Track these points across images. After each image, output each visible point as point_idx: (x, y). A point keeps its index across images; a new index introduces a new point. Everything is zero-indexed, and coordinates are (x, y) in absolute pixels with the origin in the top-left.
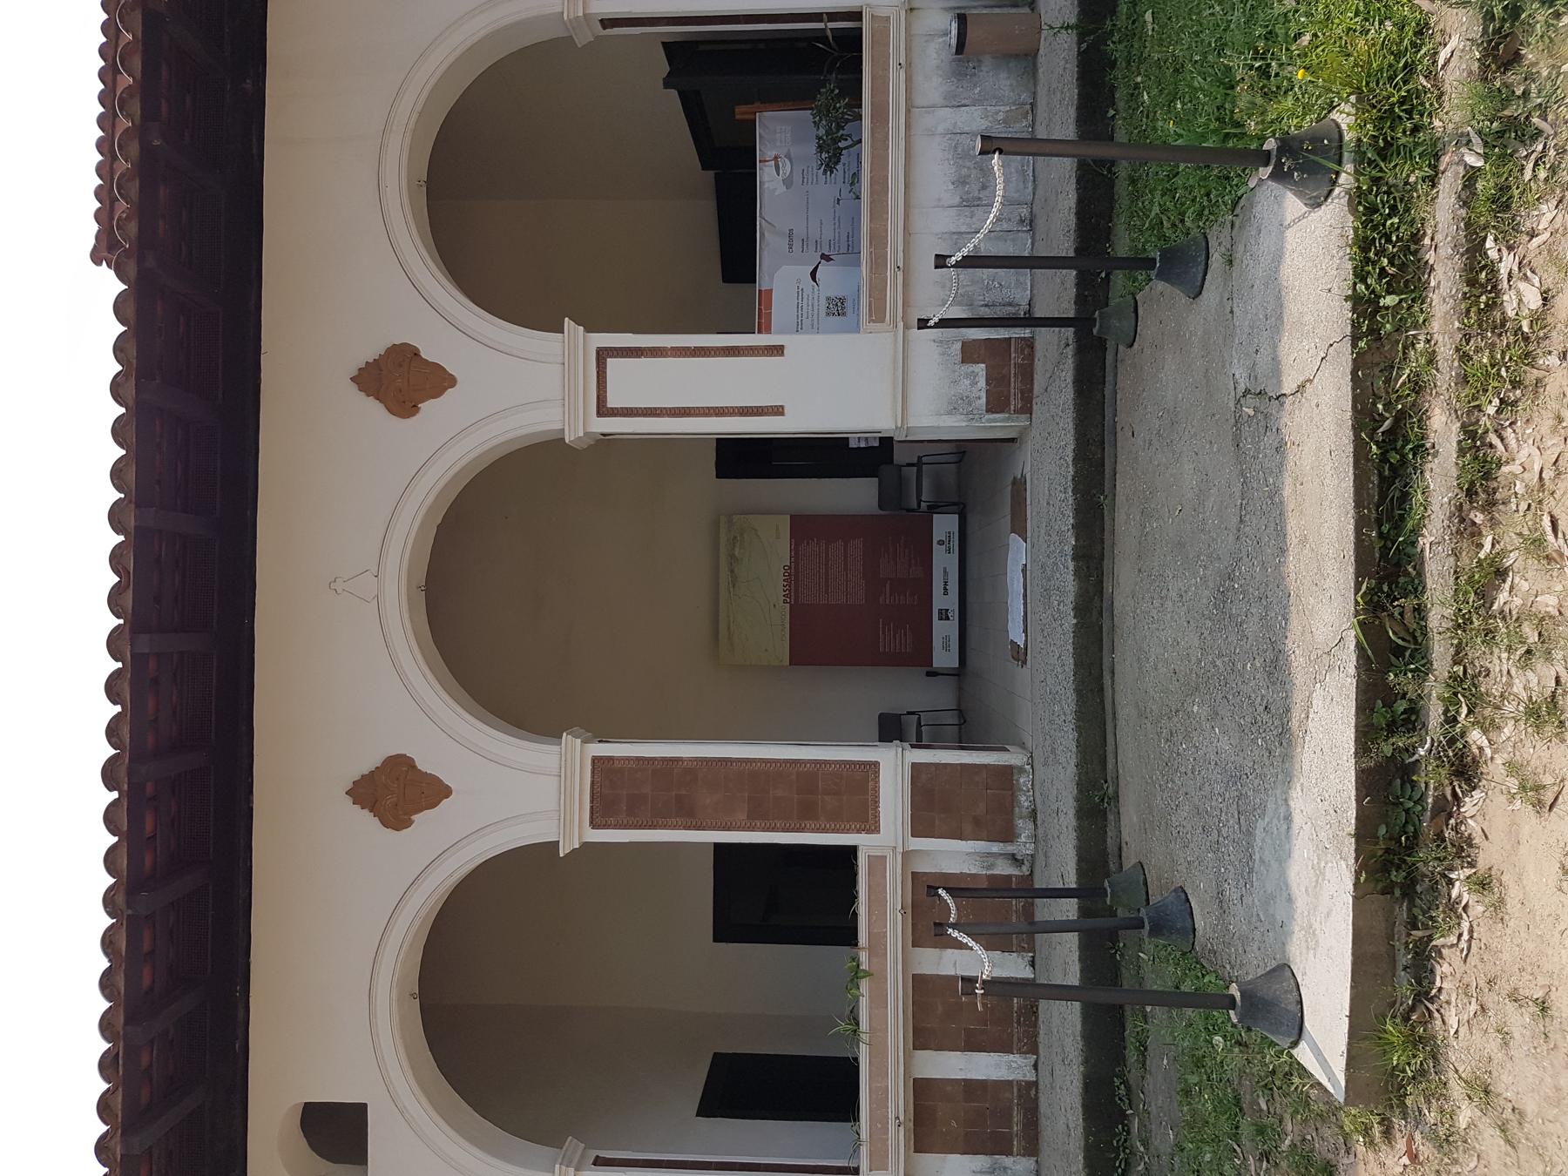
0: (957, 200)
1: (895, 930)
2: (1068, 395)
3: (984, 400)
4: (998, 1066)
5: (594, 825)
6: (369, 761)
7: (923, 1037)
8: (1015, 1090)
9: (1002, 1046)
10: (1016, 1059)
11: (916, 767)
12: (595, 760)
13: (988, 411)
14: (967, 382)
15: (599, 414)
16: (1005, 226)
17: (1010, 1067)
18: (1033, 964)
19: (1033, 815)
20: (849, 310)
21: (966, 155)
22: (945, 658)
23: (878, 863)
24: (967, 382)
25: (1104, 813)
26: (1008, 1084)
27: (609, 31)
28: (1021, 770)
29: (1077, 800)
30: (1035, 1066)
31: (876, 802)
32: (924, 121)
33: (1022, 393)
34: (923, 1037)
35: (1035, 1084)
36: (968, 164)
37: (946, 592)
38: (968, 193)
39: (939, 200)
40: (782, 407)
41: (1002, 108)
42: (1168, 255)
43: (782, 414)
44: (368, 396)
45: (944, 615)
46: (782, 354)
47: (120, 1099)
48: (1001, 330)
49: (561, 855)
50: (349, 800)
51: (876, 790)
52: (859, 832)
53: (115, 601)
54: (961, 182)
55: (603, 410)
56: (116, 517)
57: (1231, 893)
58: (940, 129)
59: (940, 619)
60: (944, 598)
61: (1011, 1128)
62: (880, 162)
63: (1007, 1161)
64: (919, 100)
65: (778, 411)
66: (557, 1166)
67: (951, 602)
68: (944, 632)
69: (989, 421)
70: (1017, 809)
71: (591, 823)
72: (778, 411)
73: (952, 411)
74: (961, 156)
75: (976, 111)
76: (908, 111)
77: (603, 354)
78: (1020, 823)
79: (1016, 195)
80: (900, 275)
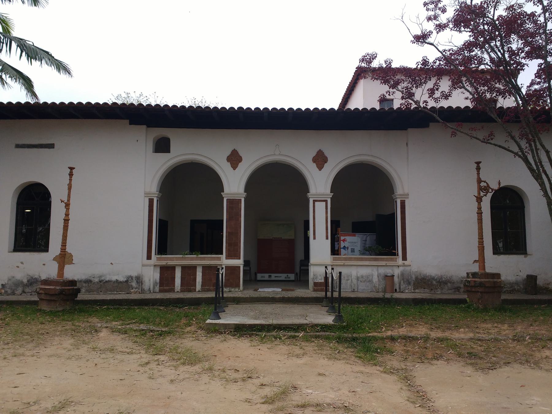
0: (358, 276)
1: (199, 263)
2: (315, 296)
3: (316, 281)
4: (178, 284)
5: (227, 200)
6: (241, 153)
7: (184, 268)
8: (173, 288)
9: (182, 284)
10: (179, 288)
11: (240, 267)
12: (241, 200)
13: (314, 282)
14: (320, 278)
15: (313, 200)
16: (353, 286)
17: (178, 286)
18: (199, 291)
19: (230, 291)
20: (352, 253)
21: (368, 278)
22: (259, 276)
23: (219, 259)
24: (320, 278)
25: (234, 302)
26: (174, 286)
27: (395, 202)
28: (239, 289)
29: (236, 297)
30: (178, 292)
31: (232, 259)
32: (375, 269)
33: (318, 290)
34: (184, 268)
35: (174, 292)
36: (366, 278)
37: (275, 277)
38: (360, 278)
39: (358, 272)
40: (315, 239)
41: (378, 285)
42: (379, 350)
43: (314, 239)
44: (317, 153)
45: (270, 276)
46: (326, 239)
47: (176, 109)
48: (331, 285)
49: (221, 193)
50: (233, 149)
51: (234, 259)
52: (226, 255)
53: (274, 109)
54: (362, 277)
55: (314, 201)
56: (291, 109)
57: (228, 314)
58: (373, 272)
59: (269, 275)
60: (274, 276)
61: (165, 287)
62: (366, 260)
63: (158, 286)
64: (379, 268)
65: (314, 238)
66: (158, 193)
67: (273, 278)
68: (266, 276)
69: (312, 282)
70: (231, 288)
71: (228, 199)
72: (314, 238)
73: (314, 275)
74: (368, 277)
75: (377, 280)
76: (377, 266)
77: (326, 201)
78: (228, 289)
79: (359, 288)
80: (343, 264)
